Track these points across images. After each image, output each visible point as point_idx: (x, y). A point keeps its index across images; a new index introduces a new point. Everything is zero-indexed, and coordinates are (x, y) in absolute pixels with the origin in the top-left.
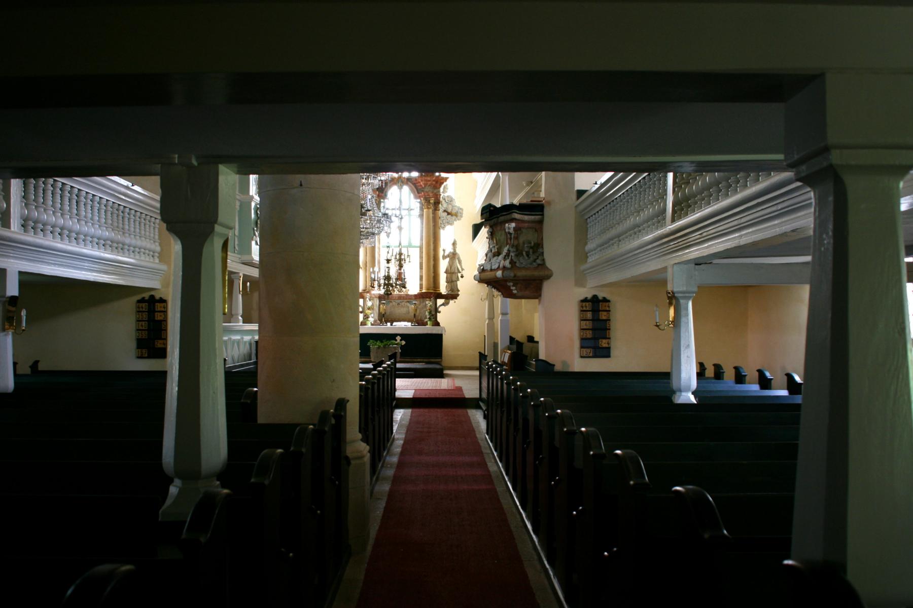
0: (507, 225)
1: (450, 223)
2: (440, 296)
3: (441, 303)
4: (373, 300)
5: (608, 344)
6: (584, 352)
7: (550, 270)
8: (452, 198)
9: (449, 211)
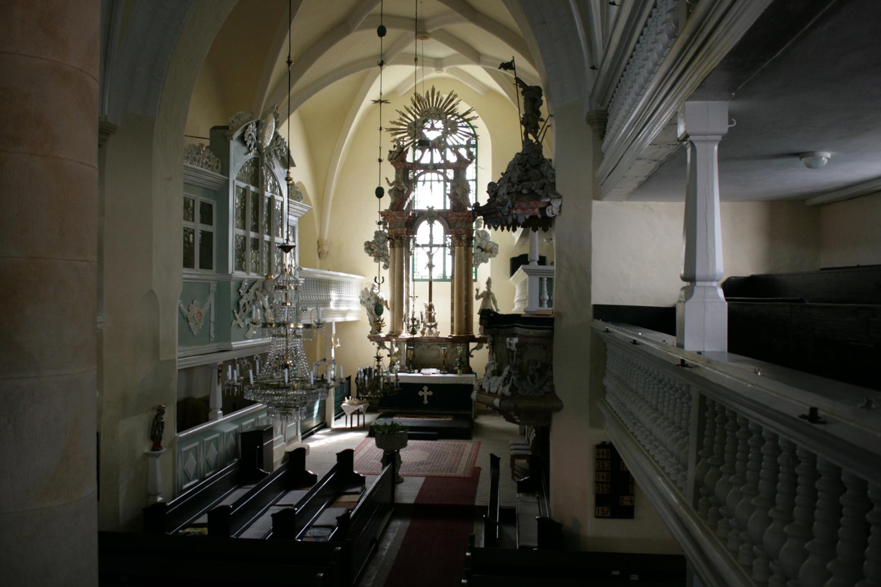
0: (508, 339)
2: (473, 339)
5: (631, 501)
6: (600, 511)
7: (560, 401)
9: (483, 247)
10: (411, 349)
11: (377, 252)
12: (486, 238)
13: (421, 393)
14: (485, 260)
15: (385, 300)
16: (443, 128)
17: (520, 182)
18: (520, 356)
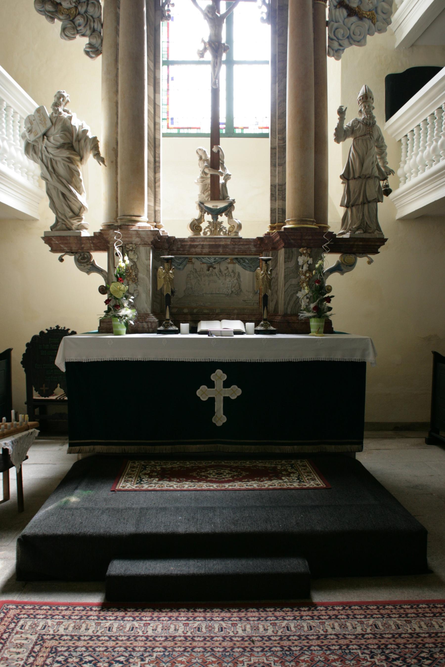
4: (135, 250)
11: (69, 9)
14: (357, 38)
15: (90, 135)
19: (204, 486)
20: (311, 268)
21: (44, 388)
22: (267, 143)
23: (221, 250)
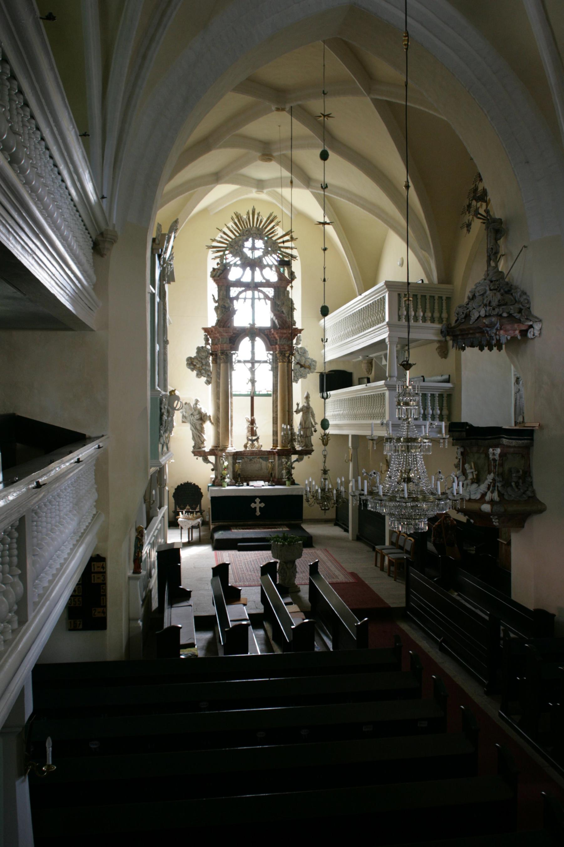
0: (491, 450)
1: (304, 376)
2: (296, 452)
3: (295, 459)
8: (305, 350)
9: (302, 363)
10: (239, 462)
11: (199, 367)
12: (305, 355)
13: (253, 505)
14: (304, 375)
15: (208, 415)
16: (264, 248)
17: (499, 306)
18: (501, 465)
19: (256, 530)
20: (287, 463)
21: (182, 506)
22: (270, 399)
23: (255, 454)
